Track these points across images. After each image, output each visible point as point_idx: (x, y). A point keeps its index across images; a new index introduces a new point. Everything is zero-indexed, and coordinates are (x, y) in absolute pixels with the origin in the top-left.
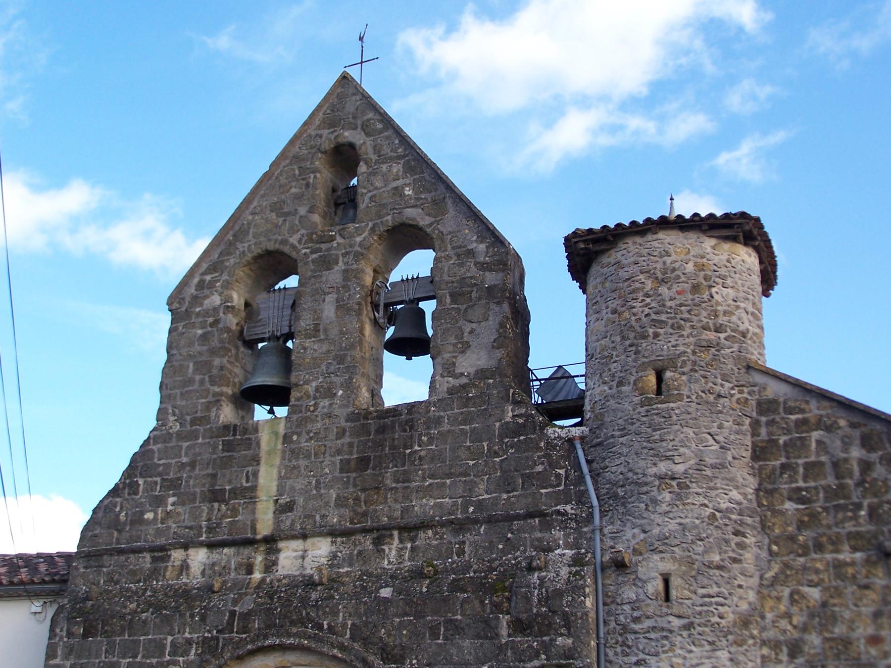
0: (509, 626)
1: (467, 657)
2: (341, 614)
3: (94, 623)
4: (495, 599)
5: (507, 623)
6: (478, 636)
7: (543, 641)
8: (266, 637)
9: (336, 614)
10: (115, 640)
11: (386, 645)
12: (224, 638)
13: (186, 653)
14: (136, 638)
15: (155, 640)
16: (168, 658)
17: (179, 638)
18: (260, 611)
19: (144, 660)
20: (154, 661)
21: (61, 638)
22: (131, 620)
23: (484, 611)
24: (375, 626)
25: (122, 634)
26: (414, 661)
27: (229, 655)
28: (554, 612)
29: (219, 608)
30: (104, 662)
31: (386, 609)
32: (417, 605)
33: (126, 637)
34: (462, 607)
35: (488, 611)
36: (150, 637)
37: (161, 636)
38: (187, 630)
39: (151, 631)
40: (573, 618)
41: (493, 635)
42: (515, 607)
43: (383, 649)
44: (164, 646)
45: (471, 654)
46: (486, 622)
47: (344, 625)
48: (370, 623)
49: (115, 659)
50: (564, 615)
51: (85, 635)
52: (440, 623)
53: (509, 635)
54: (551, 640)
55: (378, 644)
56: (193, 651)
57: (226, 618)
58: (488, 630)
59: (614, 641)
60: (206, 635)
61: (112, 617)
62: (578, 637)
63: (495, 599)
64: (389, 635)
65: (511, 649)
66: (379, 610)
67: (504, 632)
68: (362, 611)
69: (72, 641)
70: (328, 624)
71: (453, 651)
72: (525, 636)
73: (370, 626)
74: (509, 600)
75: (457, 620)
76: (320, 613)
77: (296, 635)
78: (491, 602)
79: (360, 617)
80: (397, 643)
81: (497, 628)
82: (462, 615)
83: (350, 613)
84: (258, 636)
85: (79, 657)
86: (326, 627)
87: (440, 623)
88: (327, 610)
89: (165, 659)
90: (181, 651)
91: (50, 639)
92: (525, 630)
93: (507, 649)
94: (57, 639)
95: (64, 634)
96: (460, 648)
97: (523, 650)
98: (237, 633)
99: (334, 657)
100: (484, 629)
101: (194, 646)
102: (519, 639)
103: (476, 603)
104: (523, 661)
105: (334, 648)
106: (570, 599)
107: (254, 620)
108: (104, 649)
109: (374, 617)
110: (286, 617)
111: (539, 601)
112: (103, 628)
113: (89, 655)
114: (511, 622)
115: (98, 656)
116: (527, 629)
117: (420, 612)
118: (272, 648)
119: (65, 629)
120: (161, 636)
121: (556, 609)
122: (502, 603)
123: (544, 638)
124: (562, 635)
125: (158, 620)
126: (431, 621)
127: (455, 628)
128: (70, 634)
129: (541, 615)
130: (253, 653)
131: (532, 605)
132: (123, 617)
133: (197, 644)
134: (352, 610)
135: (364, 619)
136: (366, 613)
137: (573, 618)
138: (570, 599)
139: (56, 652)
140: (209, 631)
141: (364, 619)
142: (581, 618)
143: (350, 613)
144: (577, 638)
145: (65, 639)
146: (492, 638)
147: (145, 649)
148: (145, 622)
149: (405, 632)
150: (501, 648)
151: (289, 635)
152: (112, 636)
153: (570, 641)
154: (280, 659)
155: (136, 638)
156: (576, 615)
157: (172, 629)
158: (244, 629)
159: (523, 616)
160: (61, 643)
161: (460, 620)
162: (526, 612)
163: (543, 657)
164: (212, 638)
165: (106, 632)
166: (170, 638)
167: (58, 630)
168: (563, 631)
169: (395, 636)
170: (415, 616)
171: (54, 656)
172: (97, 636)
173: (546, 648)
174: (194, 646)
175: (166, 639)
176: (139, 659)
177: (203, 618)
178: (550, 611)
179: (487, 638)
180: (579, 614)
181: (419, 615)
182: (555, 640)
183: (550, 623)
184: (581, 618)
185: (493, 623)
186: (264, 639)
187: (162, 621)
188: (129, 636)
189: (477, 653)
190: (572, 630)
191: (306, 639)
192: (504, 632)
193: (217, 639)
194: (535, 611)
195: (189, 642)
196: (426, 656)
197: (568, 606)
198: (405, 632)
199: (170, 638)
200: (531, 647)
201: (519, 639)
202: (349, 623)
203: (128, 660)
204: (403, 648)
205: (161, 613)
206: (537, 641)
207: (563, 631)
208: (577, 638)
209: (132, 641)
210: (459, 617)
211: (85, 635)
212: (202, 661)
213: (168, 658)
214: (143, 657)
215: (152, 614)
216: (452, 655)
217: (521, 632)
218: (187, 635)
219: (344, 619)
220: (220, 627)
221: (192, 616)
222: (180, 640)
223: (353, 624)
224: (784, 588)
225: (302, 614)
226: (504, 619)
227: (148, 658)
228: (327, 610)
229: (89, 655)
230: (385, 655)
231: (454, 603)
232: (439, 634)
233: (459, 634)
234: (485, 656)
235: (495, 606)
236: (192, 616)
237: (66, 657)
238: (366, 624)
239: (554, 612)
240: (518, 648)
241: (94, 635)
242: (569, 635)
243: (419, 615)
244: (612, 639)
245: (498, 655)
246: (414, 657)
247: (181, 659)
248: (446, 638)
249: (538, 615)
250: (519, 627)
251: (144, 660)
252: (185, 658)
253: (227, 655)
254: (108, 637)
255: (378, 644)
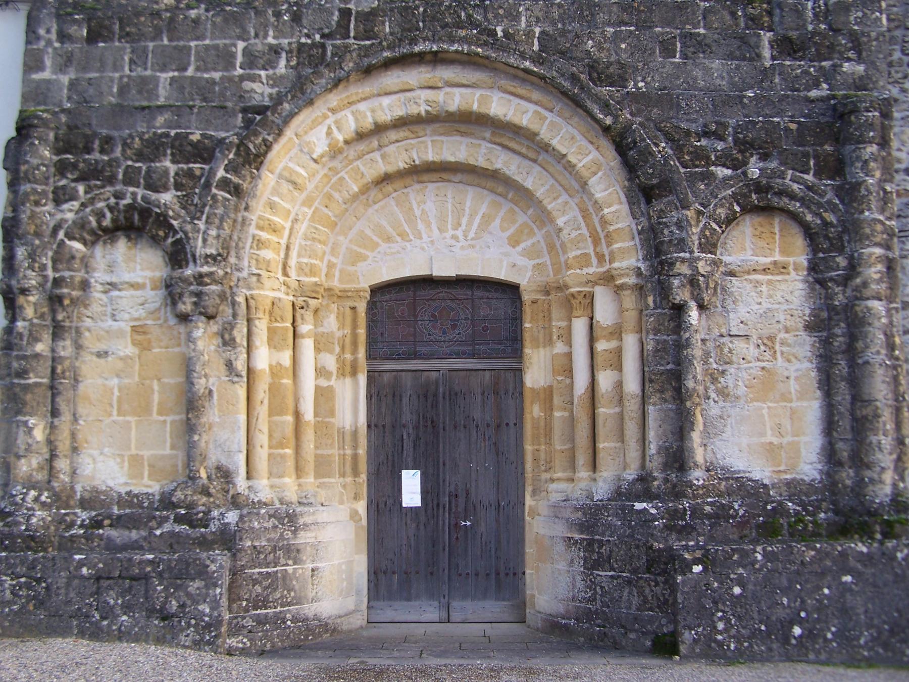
0: (772, 47)
1: (718, 82)
2: (523, 19)
3: (107, 22)
4: (752, 11)
5: (769, 42)
6: (731, 57)
7: (821, 67)
8: (413, 41)
9: (516, 18)
10: (146, 47)
11: (595, 61)
12: (333, 46)
13: (270, 64)
14: (181, 43)
15: (216, 47)
16: (239, 71)
17: (258, 45)
18: (392, 10)
19: (199, 74)
20: (217, 75)
21: (49, 43)
22: (172, 20)
23: (737, 25)
24: (577, 36)
25: (157, 36)
26: (641, 84)
27: (351, 65)
28: (837, 31)
29: (320, 5)
30: (129, 77)
31: (592, 15)
32: (639, 11)
33: (166, 42)
34: (704, 18)
35: (742, 25)
36: (207, 42)
37: (227, 42)
38: (271, 33)
39: (208, 34)
40: (865, 39)
41: (754, 55)
42: (781, 23)
43: (592, 67)
44: (233, 56)
45: (723, 78)
46: (743, 39)
47: (529, 34)
48: (570, 32)
49: (148, 73)
50: (851, 35)
51: (92, 38)
52: (675, 37)
53: (773, 58)
54: (834, 66)
55: (583, 59)
56: (283, 62)
57: (335, 18)
58: (746, 49)
59: (900, 75)
60: (303, 40)
61: (138, 14)
62: (873, 63)
63: (752, 11)
64: (600, 49)
65: (779, 74)
66: (582, 16)
67: (766, 53)
68: (556, 15)
69: (69, 47)
70: (503, 31)
71: (698, 73)
72: (795, 59)
73: (570, 36)
74: (770, 13)
75: (699, 34)
76: (490, 16)
77: (462, 40)
78: (745, 15)
79: (554, 23)
80: (612, 59)
81: (758, 47)
82: (705, 27)
83: (538, 18)
84: (400, 40)
85: (85, 69)
86: (500, 34)
87: (675, 37)
88: (501, 12)
89: (236, 73)
90: (261, 61)
91: (28, 42)
92: (795, 52)
93: (773, 75)
94: (42, 43)
95: (54, 36)
96: (707, 70)
97: (796, 77)
98: (355, 38)
99: (526, 71)
100: (739, 47)
101: (284, 55)
102: (788, 63)
103: (726, 14)
104: (798, 90)
105: (525, 59)
106: (860, 14)
107: (383, 23)
108: (127, 58)
109: (575, 25)
110: (434, 18)
111: (816, 15)
112: (122, 28)
113: (102, 66)
114: (774, 41)
115: (116, 68)
116: (799, 50)
117: (645, 22)
118: (419, 59)
119: (54, 30)
120: (227, 42)
121: (840, 27)
122: (762, 16)
123: (824, 63)
124: (849, 60)
125: (218, 20)
126: (662, 34)
127: (697, 46)
128: (63, 37)
129: (820, 34)
130: (388, 64)
131: (806, 21)
132: (157, 14)
133: (290, 52)
134: (540, 14)
135: (560, 26)
136: (562, 19)
137: (865, 39)
138: (860, 14)
139: (42, 62)
140: (308, 36)
141: (560, 26)
142: (877, 39)
143: (538, 18)
144: (871, 64)
145: (57, 45)
146: (751, 60)
147: (199, 58)
148: (196, 22)
149: (623, 46)
150: (766, 73)
151: (452, 40)
152: (139, 40)
153: (861, 68)
154: (428, 76)
155: (181, 43)
156: (869, 36)
157: (245, 30)
158: (368, 34)
159: (794, 34)
160: (50, 50)
161: (704, 35)
162: (797, 30)
163: (825, 86)
164: (314, 45)
165: (128, 34)
166: (241, 45)
167: (42, 32)
168: (851, 54)
169: (608, 50)
170: (636, 26)
171: (40, 68)
172: (112, 40)
173: (828, 76)
174: (284, 55)
175: (235, 46)
176: (190, 72)
177: (296, 18)
178: (831, 29)
179: (744, 59)
180: (873, 34)
181: (644, 26)
182: (841, 66)
183: (832, 44)
184: (877, 39)
185: (753, 40)
186: (410, 44)
187: (226, 20)
188: (170, 40)
189: (731, 77)
190: (864, 54)
191: (480, 46)
192: (766, 53)
193: (323, 46)
194: (810, 28)
195: (275, 51)
196: (657, 77)
197: (857, 24)
198: (623, 46)
199: (241, 45)
200: (806, 73)
201: (788, 63)
202: (537, 30)
203: (171, 74)
204: (622, 66)
205: (223, 10)
206: (814, 66)
207: (851, 54)
208: (871, 64)
209: (175, 48)
210: (702, 31)
211: (92, 38)
212: (299, 77)
213: (239, 71)
214: (198, 69)
215: (207, 10)
216: (695, 79)
217: (789, 55)
218: (270, 40)
219: (529, 24)
220: (326, 31)
221: (278, 15)
222: (260, 47)
223: (542, 33)
224: (591, 147)
225: (459, 17)
226: (766, 37)
227: (207, 70)
228: (501, 12)
229: (102, 66)
230: (595, 75)
231: (694, 13)
232: (675, 51)
233: (704, 52)
234: (743, 82)
235: (752, 20)
236: (278, 15)
237: (61, 68)
238: (563, 33)
239: (837, 31)
240: (789, 74)
241: (109, 39)
242: (859, 60)
243: (644, 26)
244: (897, 72)
245: (762, 81)
246: (640, 78)
247: (263, 73)
248: (685, 56)
249: (815, 33)
250: (787, 47)
251: (199, 74)
252: (271, 72)
253: (349, 65)
254: (133, 41)
255: (583, 59)
